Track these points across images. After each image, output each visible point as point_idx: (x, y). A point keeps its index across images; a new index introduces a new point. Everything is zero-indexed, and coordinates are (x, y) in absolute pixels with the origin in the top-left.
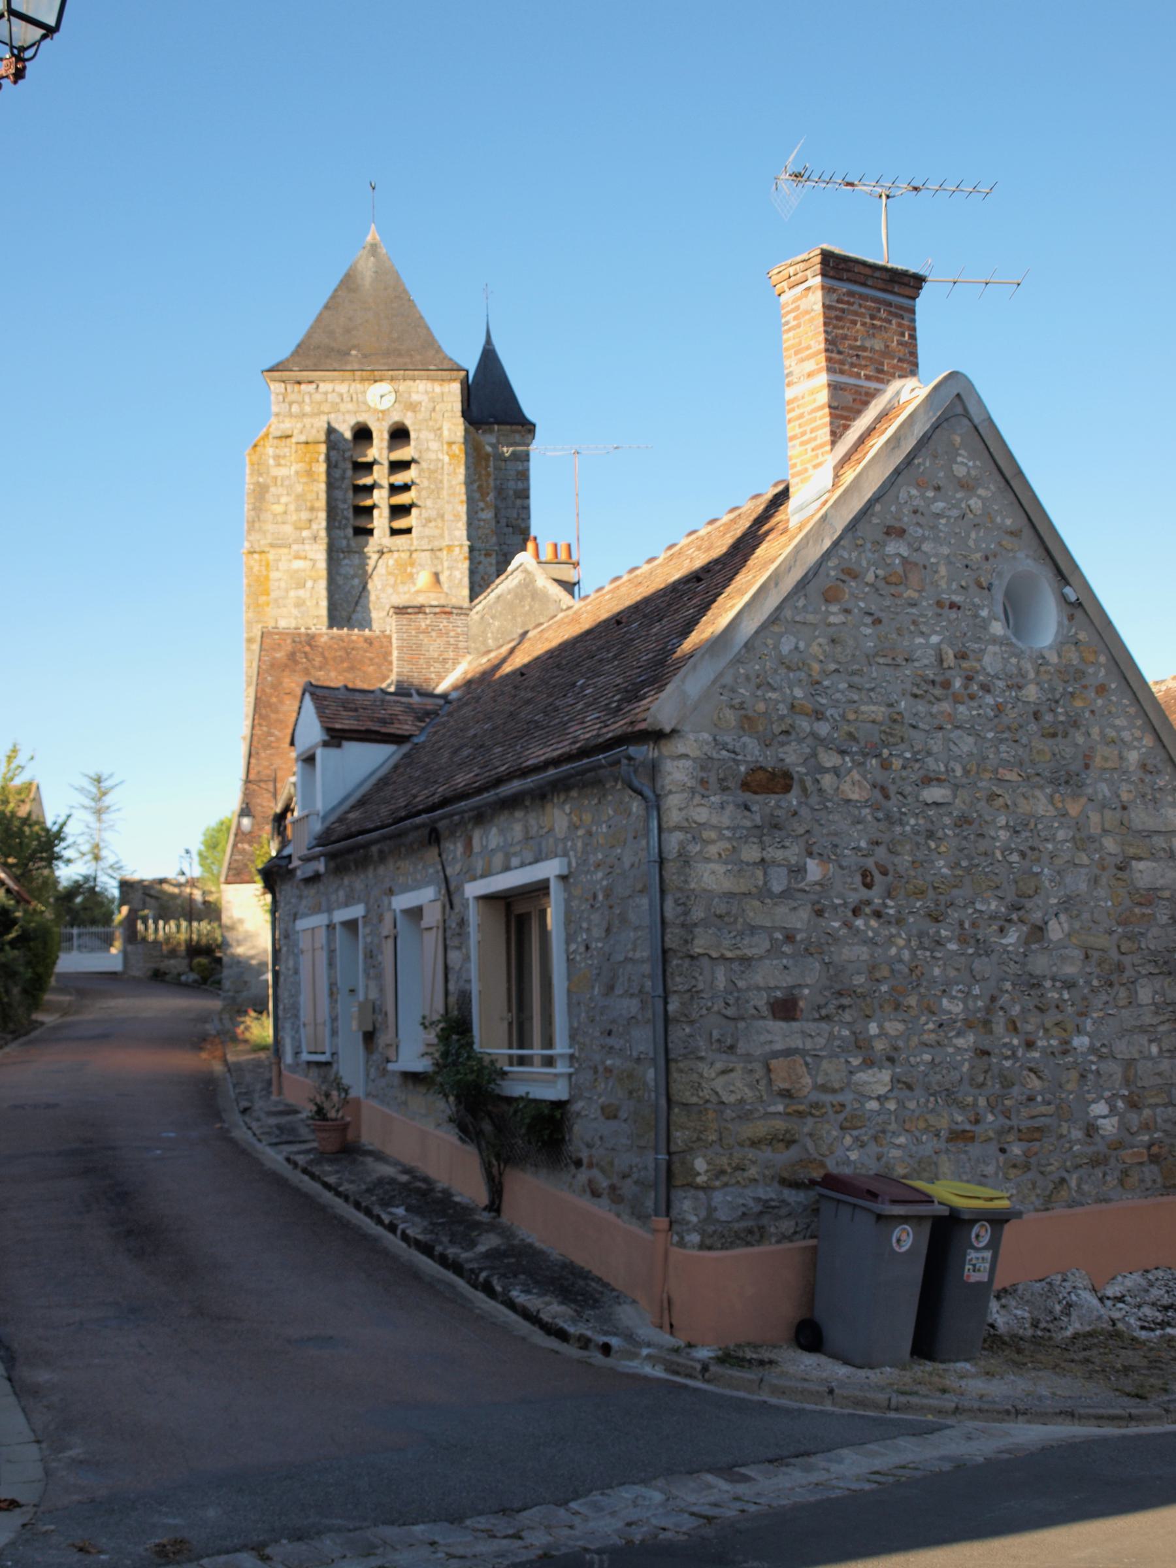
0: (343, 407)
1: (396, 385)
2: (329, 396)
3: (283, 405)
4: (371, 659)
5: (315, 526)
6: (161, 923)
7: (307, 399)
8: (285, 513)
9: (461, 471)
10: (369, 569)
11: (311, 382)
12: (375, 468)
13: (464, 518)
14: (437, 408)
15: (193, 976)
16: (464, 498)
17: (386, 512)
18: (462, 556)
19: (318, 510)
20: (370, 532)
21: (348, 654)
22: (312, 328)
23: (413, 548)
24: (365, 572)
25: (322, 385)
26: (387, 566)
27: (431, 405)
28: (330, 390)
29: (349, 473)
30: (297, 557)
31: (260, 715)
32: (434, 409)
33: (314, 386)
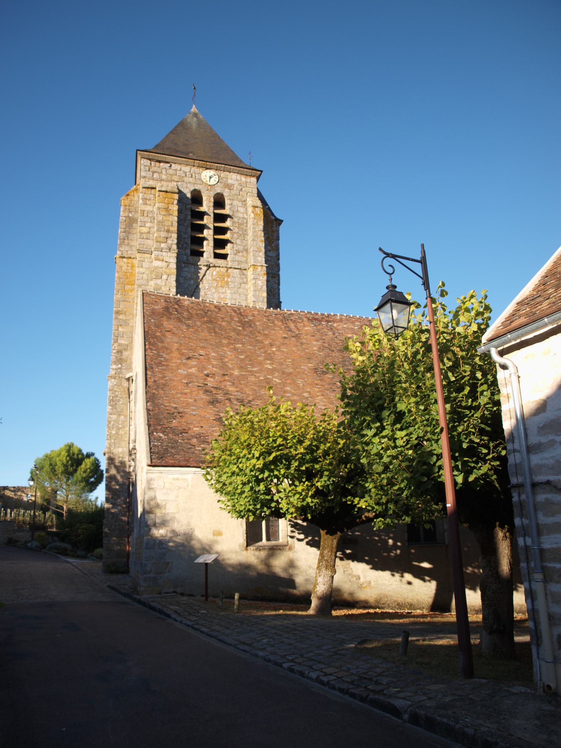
0: (186, 179)
1: (219, 172)
2: (178, 172)
3: (148, 173)
4: (222, 318)
5: (169, 242)
6: (9, 511)
7: (164, 171)
8: (149, 233)
9: (261, 223)
10: (201, 275)
11: (168, 163)
12: (205, 217)
13: (263, 250)
14: (243, 189)
15: (35, 544)
16: (263, 239)
17: (212, 243)
18: (262, 273)
19: (172, 232)
20: (201, 254)
21: (206, 313)
22: (164, 139)
23: (228, 266)
24: (198, 277)
25: (173, 165)
26: (212, 275)
27: (240, 187)
28: (179, 169)
29: (189, 217)
30: (157, 259)
31: (150, 342)
32: (241, 190)
33: (169, 165)
